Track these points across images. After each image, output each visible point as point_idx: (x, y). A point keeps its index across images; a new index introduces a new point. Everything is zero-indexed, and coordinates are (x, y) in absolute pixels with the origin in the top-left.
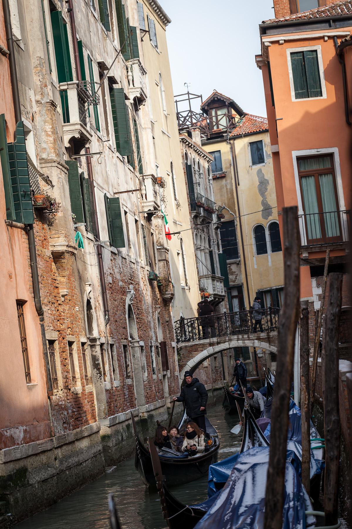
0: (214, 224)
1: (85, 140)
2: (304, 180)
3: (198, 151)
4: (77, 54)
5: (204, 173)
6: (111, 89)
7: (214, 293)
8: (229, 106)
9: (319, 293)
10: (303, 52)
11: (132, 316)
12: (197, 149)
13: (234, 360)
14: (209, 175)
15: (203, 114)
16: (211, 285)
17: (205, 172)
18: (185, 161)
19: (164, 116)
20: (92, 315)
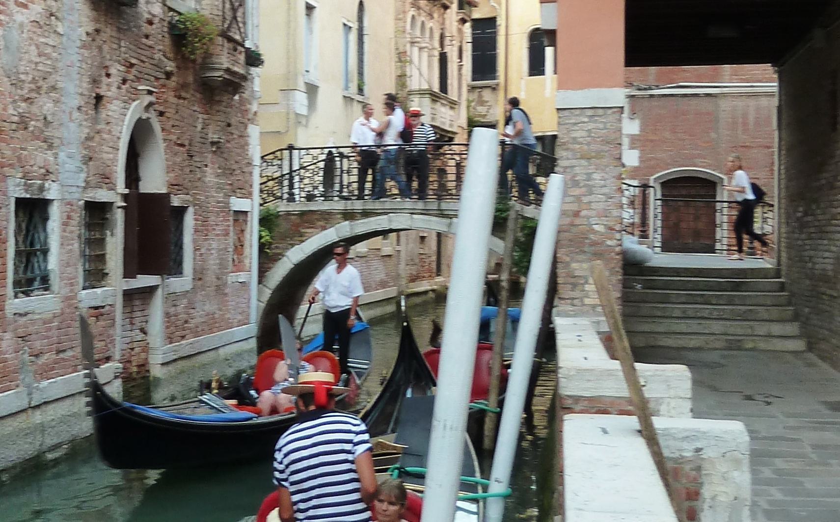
9: (633, 133)
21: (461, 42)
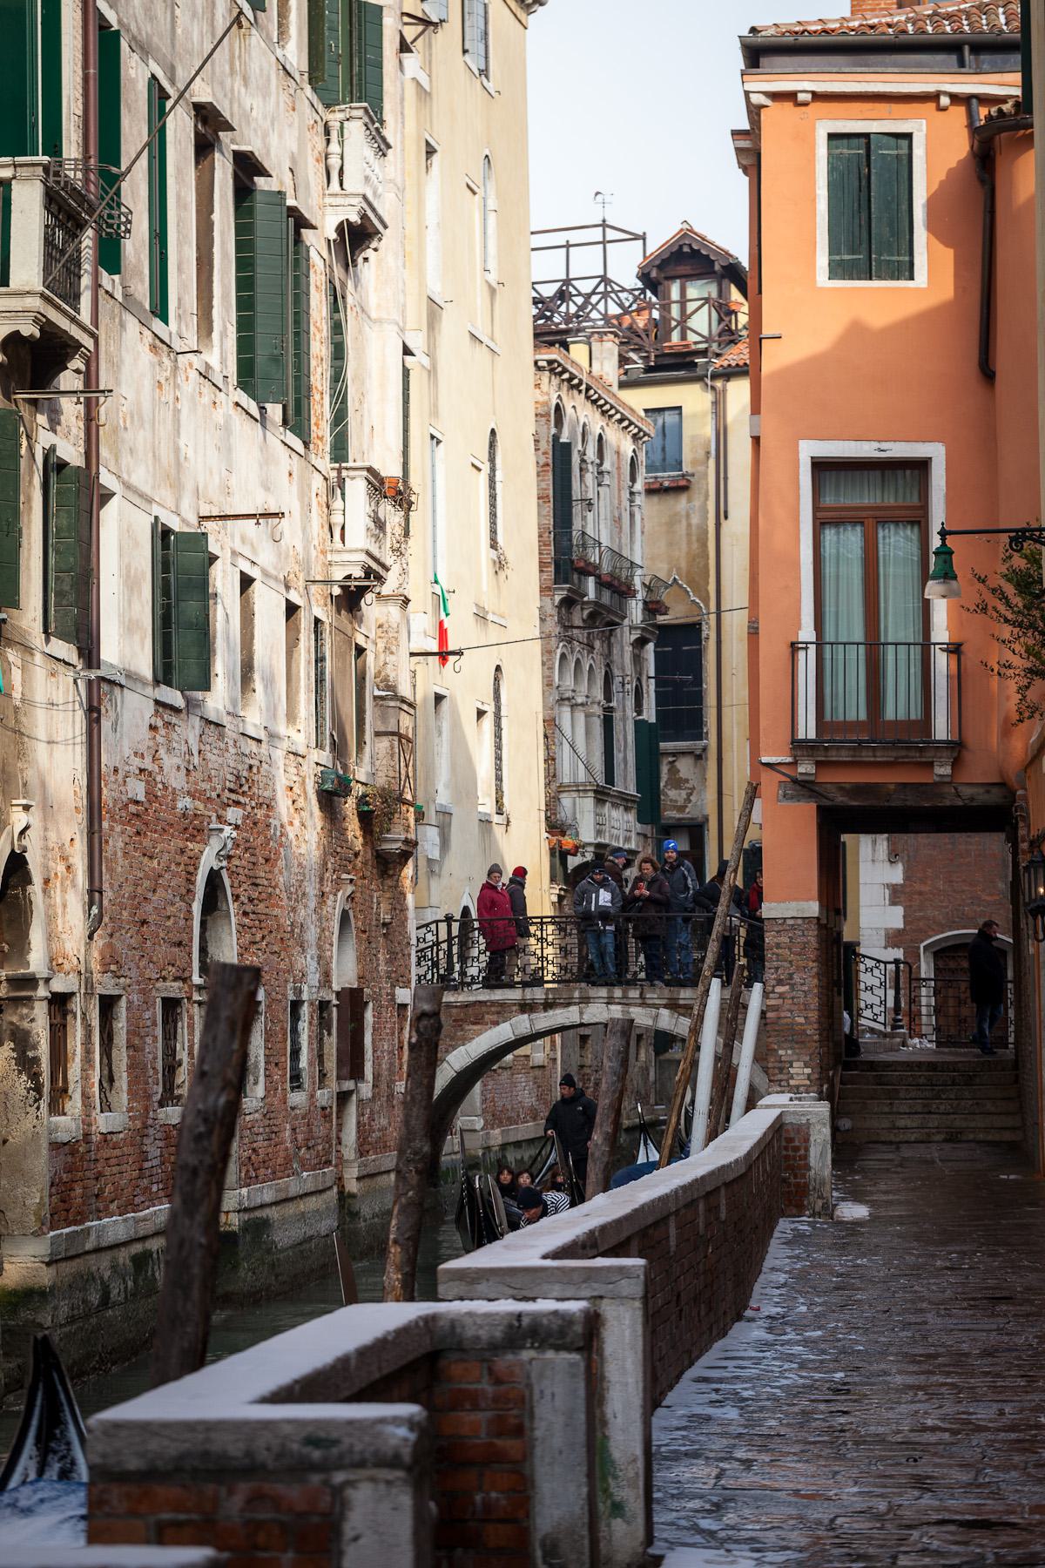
0: (631, 628)
1: (69, 346)
2: (829, 535)
3: (602, 402)
4: (92, 71)
5: (615, 472)
6: (243, 192)
7: (599, 840)
8: (723, 277)
9: (894, 882)
10: (867, 136)
11: (224, 908)
12: (600, 398)
13: (651, 1049)
14: (633, 479)
15: (643, 291)
16: (592, 815)
17: (619, 468)
18: (553, 431)
19: (486, 288)
20: (31, 902)
21: (639, 680)
